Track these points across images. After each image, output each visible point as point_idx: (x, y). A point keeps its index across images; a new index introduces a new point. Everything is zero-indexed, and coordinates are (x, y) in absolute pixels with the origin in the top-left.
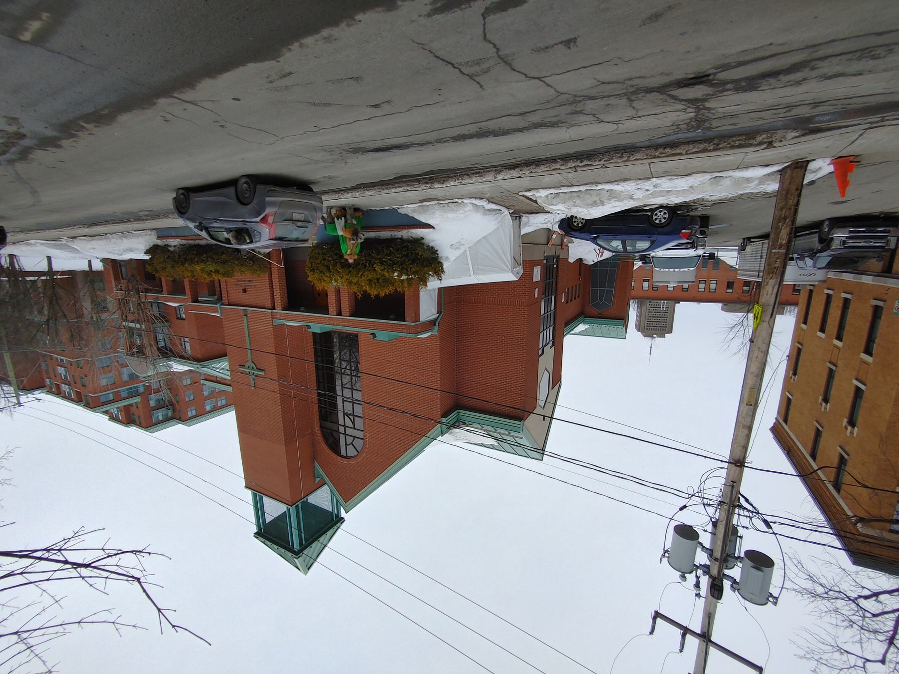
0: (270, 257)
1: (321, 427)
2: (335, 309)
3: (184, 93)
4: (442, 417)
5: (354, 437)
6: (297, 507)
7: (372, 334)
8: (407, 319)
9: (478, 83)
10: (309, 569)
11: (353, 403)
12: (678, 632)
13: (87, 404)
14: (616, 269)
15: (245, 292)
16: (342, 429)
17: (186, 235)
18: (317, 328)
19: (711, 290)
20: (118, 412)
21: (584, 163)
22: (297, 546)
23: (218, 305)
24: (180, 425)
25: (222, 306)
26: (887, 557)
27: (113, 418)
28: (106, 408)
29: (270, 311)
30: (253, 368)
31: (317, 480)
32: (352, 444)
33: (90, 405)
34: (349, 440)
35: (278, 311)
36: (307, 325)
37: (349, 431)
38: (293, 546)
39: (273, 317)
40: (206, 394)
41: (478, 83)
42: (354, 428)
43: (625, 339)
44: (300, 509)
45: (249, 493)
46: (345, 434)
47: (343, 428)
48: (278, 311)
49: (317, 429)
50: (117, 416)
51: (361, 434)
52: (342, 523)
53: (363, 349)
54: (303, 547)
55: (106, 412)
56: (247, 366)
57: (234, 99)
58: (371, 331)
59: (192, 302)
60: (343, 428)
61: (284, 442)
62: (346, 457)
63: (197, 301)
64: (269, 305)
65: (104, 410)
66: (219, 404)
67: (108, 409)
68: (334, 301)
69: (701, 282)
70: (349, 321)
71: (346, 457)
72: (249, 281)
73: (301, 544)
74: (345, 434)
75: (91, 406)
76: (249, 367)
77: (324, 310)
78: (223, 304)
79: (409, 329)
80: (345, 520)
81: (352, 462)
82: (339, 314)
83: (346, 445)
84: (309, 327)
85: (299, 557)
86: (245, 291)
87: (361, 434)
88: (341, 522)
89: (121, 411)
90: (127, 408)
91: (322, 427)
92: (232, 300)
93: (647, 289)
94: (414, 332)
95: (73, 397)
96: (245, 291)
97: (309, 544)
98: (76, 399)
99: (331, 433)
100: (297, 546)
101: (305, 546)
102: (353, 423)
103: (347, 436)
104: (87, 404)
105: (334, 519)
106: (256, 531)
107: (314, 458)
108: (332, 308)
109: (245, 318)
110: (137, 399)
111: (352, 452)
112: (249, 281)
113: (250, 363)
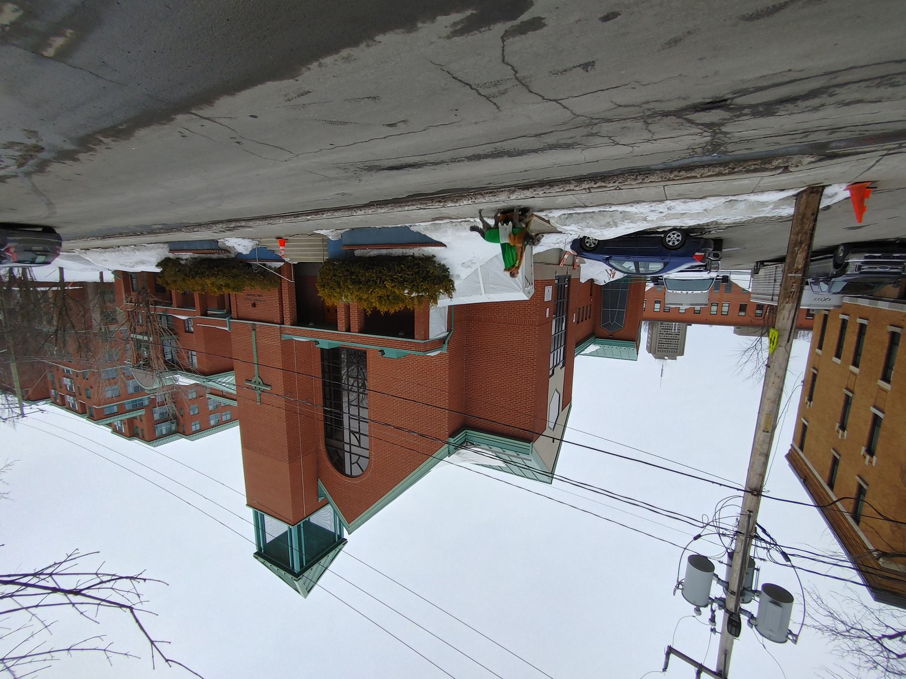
0: (281, 272)
4: (449, 437)
5: (360, 456)
7: (380, 351)
10: (309, 592)
14: (628, 290)
16: (347, 447)
17: (198, 249)
18: (325, 344)
20: (121, 425)
21: (598, 185)
22: (297, 568)
23: (227, 319)
24: (183, 439)
27: (116, 431)
29: (278, 326)
30: (259, 383)
31: (320, 499)
33: (93, 417)
34: (355, 458)
35: (287, 326)
37: (354, 449)
39: (281, 331)
40: (211, 408)
42: (360, 446)
46: (350, 452)
48: (287, 326)
49: (322, 447)
50: (120, 429)
51: (366, 453)
55: (109, 425)
56: (253, 381)
61: (288, 459)
62: (351, 476)
63: (206, 315)
64: (278, 319)
66: (224, 418)
69: (713, 304)
71: (351, 476)
72: (259, 295)
73: (301, 566)
74: (350, 452)
75: (95, 418)
76: (255, 382)
77: (334, 326)
78: (231, 318)
82: (348, 330)
83: (351, 464)
85: (299, 579)
86: (254, 305)
87: (366, 453)
89: (125, 424)
90: (131, 421)
91: (327, 445)
92: (241, 315)
93: (658, 310)
96: (254, 305)
97: (309, 567)
100: (297, 568)
102: (359, 441)
106: (256, 551)
107: (318, 474)
108: (341, 324)
109: (253, 332)
110: (142, 412)
111: (356, 471)
112: (259, 295)
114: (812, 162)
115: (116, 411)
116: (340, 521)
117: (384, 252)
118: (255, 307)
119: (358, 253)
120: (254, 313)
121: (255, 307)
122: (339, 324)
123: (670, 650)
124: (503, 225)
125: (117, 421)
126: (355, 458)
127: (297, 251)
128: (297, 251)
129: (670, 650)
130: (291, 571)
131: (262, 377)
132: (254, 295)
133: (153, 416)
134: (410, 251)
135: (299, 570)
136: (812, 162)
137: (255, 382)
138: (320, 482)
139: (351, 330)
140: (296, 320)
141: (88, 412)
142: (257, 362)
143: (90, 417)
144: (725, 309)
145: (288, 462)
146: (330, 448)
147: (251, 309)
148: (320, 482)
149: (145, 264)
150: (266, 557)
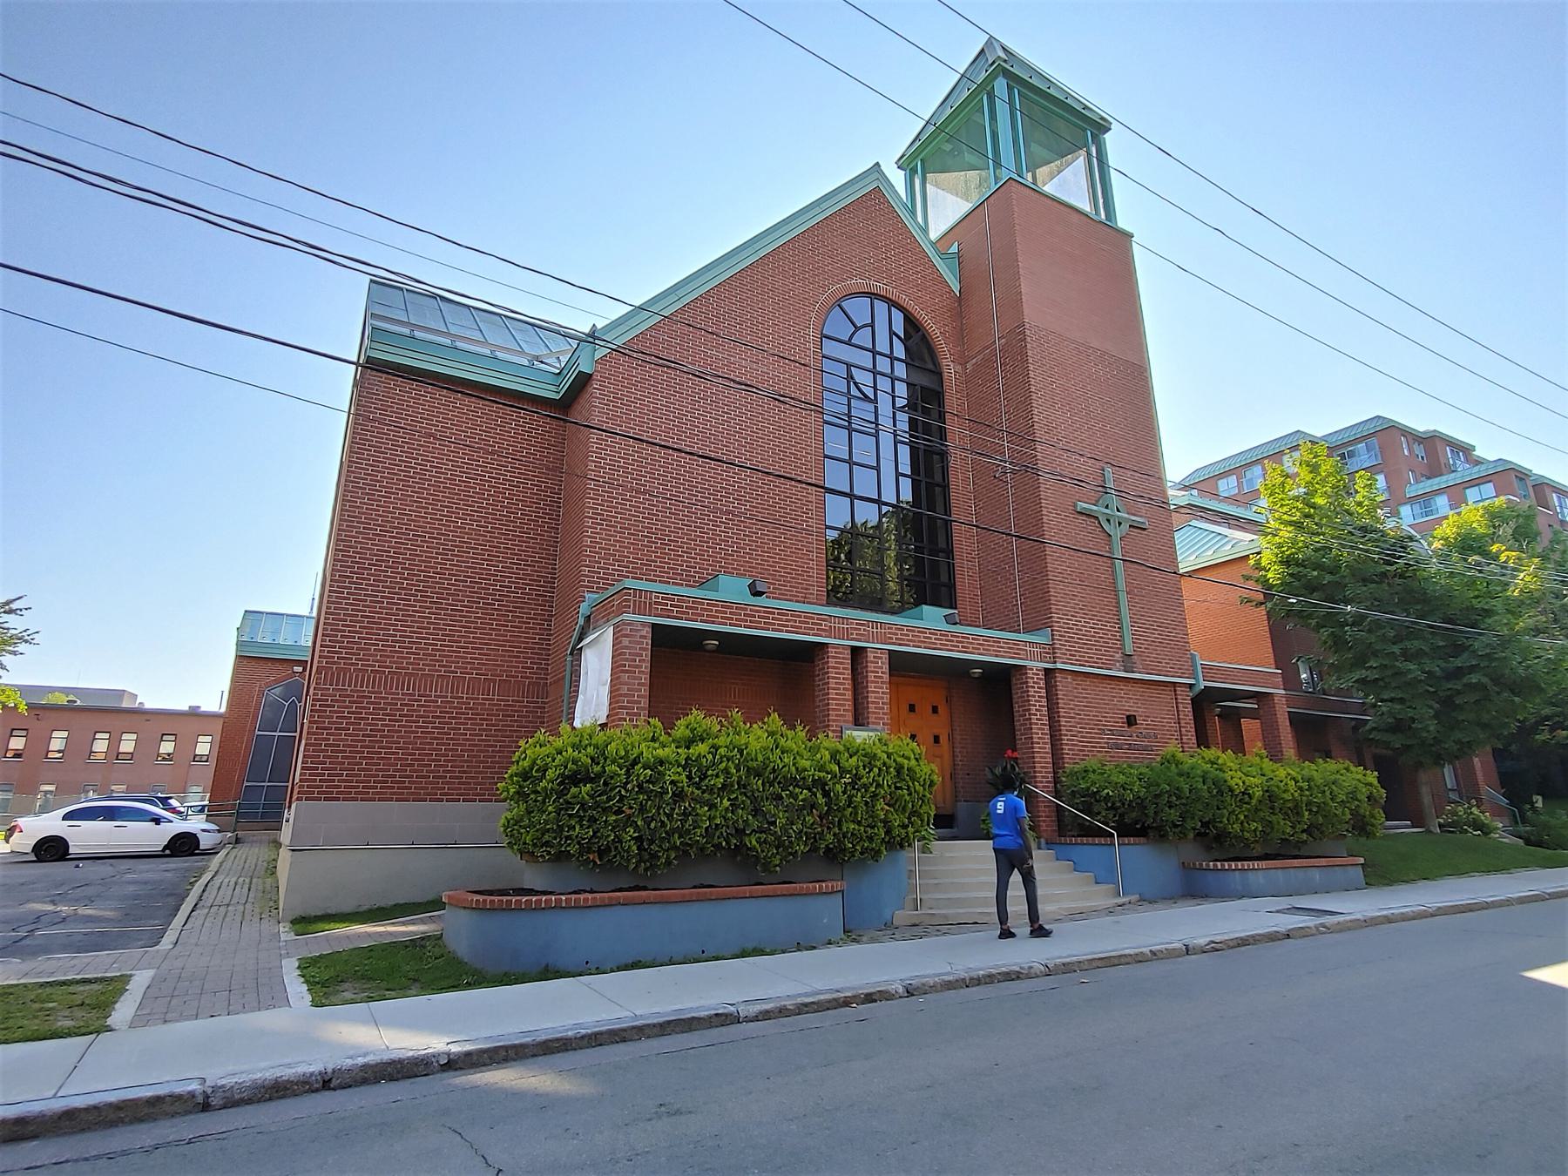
0: (1057, 811)
1: (940, 374)
2: (871, 666)
4: (591, 375)
5: (849, 343)
7: (759, 594)
8: (647, 632)
11: (850, 430)
13: (1521, 479)
14: (246, 784)
15: (1128, 717)
16: (901, 370)
17: (1280, 871)
18: (932, 617)
19: (173, 738)
20: (1455, 464)
23: (1202, 684)
25: (1192, 681)
27: (1465, 450)
28: (1477, 472)
29: (1059, 666)
30: (1108, 520)
31: (954, 249)
32: (857, 328)
33: (1516, 476)
35: (1036, 665)
36: (955, 624)
37: (865, 359)
38: (1010, 88)
39: (1051, 652)
42: (849, 366)
43: (246, 611)
45: (1122, 223)
46: (875, 353)
47: (896, 373)
48: (1036, 665)
49: (950, 369)
50: (1455, 453)
51: (830, 348)
53: (813, 564)
55: (1478, 462)
56: (1125, 527)
58: (762, 601)
60: (896, 373)
61: (1028, 332)
62: (873, 296)
64: (1063, 686)
65: (1483, 467)
66: (1233, 480)
67: (1476, 469)
68: (872, 687)
69: (129, 757)
70: (829, 632)
71: (873, 296)
72: (1118, 747)
74: (875, 353)
75: (1513, 474)
76: (1120, 524)
77: (901, 665)
78: (1191, 686)
79: (643, 603)
81: (857, 283)
82: (857, 653)
83: (872, 325)
84: (949, 619)
85: (994, 63)
86: (1131, 721)
87: (830, 348)
89: (1447, 465)
90: (1434, 470)
91: (938, 374)
92: (1167, 696)
93: (125, 736)
94: (626, 594)
95: (1554, 495)
96: (1131, 721)
98: (1547, 491)
99: (913, 360)
100: (1000, 85)
102: (850, 377)
104: (1521, 479)
106: (1107, 136)
107: (960, 305)
108: (878, 670)
109: (1129, 649)
110: (1411, 491)
111: (859, 309)
112: (1118, 747)
113: (1117, 533)
115: (1468, 491)
116: (913, 212)
120: (1131, 703)
121: (1128, 717)
122: (886, 668)
125: (1464, 471)
126: (863, 338)
130: (1007, 74)
131: (1102, 536)
132: (1130, 747)
133: (1387, 483)
135: (996, 84)
137: (1120, 524)
138: (956, 288)
140: (1014, 681)
141: (1531, 489)
142: (1113, 564)
143: (1523, 476)
144: (101, 746)
145: (1027, 326)
146: (930, 366)
147: (1139, 712)
148: (956, 288)
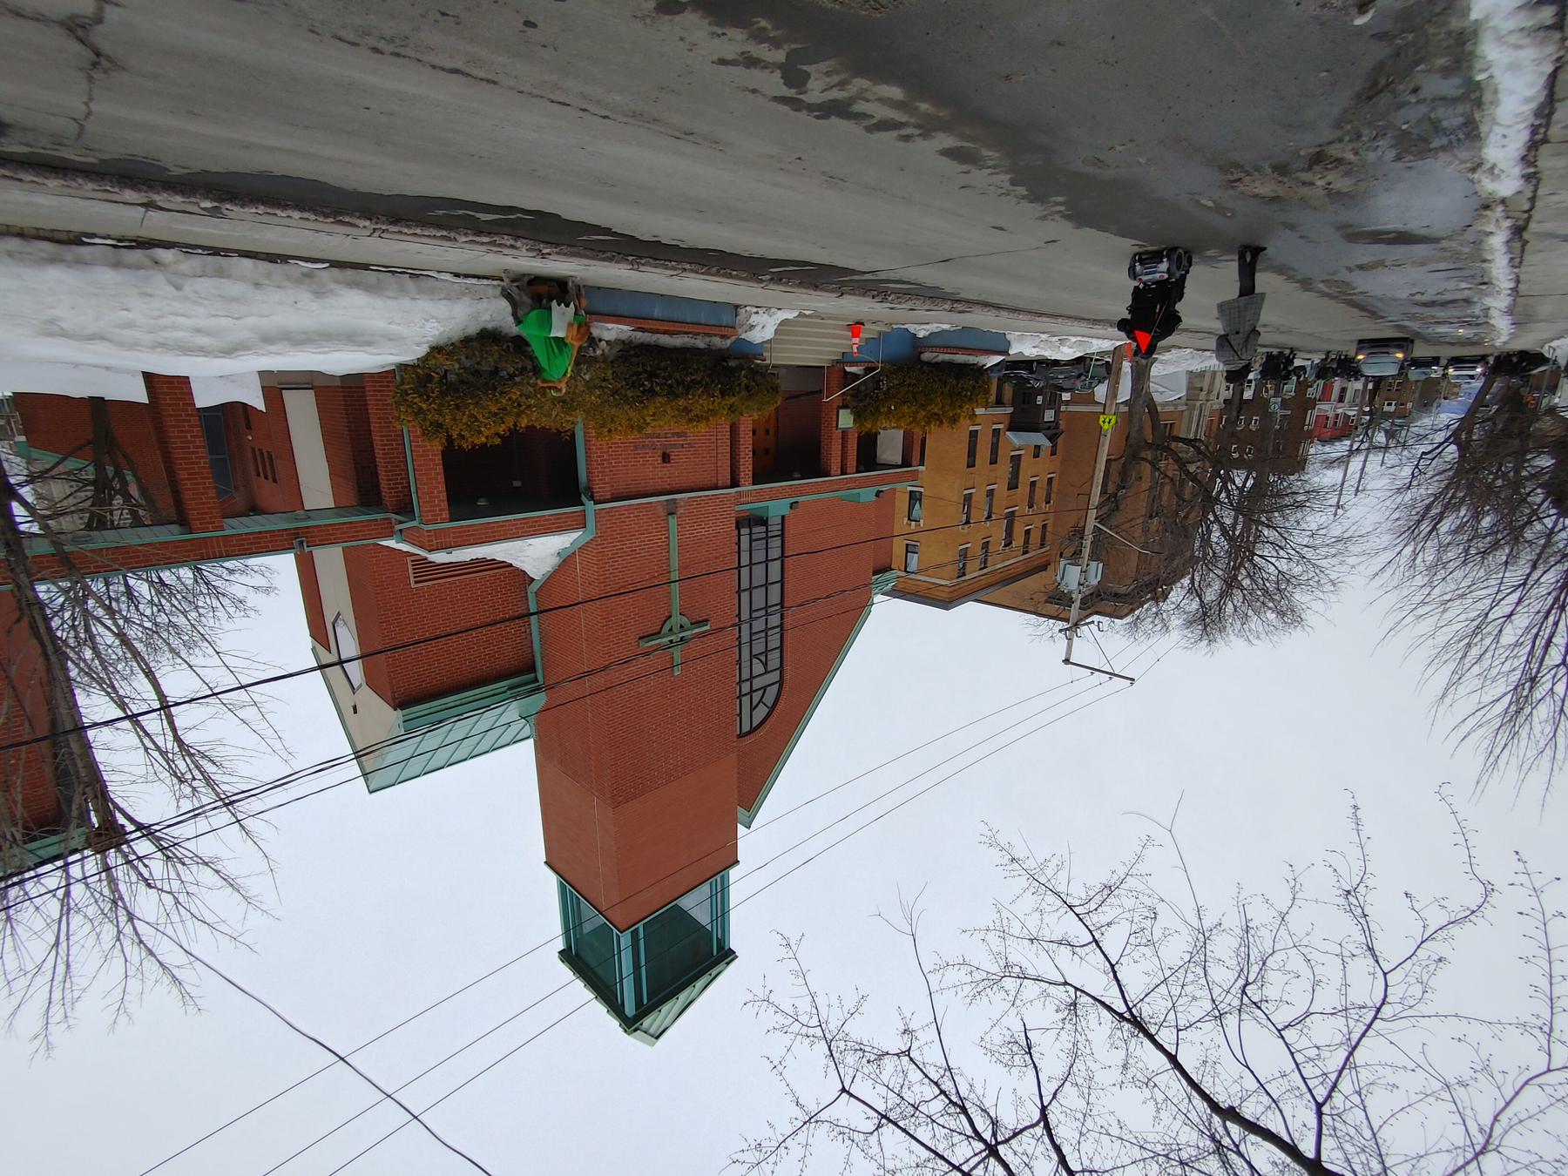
3: (1376, 196)
6: (635, 934)
9: (1381, 1127)
12: (1388, 976)
21: (412, 231)
22: (630, 1010)
26: (275, 214)
41: (1381, 1127)
44: (642, 942)
46: (751, 678)
52: (728, 964)
54: (644, 1011)
57: (355, 712)
59: (754, 484)
73: (639, 1003)
80: (737, 957)
86: (666, 458)
88: (727, 960)
100: (630, 1010)
101: (648, 1008)
103: (754, 675)
105: (715, 953)
106: (562, 948)
108: (835, 466)
114: (94, 190)
117: (947, 357)
118: (669, 462)
119: (926, 356)
121: (669, 462)
123: (1067, 661)
124: (559, 305)
127: (800, 343)
128: (800, 343)
129: (1067, 661)
134: (972, 359)
136: (94, 190)
139: (848, 471)
149: (370, 344)
150: (699, 972)
